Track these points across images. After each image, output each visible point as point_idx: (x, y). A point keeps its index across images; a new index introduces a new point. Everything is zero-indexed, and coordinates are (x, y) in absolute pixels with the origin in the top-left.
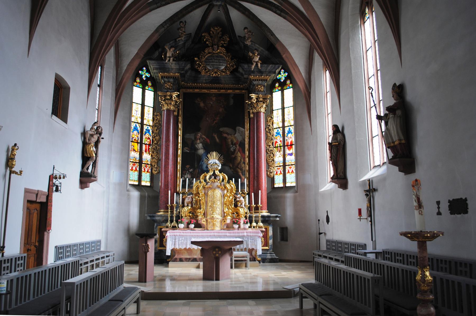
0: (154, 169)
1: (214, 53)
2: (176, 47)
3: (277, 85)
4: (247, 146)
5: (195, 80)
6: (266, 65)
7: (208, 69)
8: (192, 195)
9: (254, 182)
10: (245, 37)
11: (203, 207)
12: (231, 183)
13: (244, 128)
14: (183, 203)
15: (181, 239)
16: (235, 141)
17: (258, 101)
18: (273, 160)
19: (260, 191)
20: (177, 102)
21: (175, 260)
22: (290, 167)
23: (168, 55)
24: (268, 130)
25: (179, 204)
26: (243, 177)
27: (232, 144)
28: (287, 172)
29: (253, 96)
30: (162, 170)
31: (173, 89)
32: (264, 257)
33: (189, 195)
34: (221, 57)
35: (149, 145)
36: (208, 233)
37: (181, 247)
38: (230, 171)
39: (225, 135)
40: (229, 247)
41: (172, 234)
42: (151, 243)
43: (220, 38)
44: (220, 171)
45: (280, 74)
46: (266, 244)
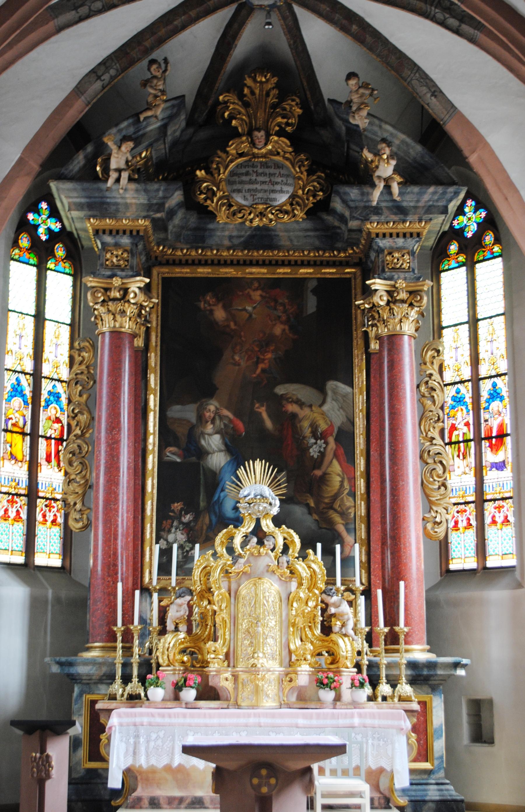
0: (74, 515)
1: (255, 156)
2: (137, 140)
3: (454, 248)
4: (360, 442)
5: (199, 237)
6: (416, 189)
7: (237, 204)
8: (188, 598)
9: (383, 553)
10: (349, 103)
12: (311, 556)
13: (351, 384)
14: (162, 620)
15: (154, 736)
16: (323, 426)
17: (392, 301)
18: (444, 485)
19: (402, 584)
20: (142, 307)
22: (499, 508)
23: (113, 164)
24: (426, 389)
25: (151, 624)
26: (349, 539)
27: (314, 434)
28: (488, 520)
29: (378, 284)
30: (97, 519)
31: (132, 268)
32: (418, 795)
33: (180, 596)
34: (278, 166)
35: (60, 440)
36: (238, 716)
37: (153, 762)
38: (310, 522)
39: (292, 408)
40: (300, 765)
41: (125, 720)
42: (58, 751)
43: (274, 106)
44: (277, 521)
46: (423, 753)
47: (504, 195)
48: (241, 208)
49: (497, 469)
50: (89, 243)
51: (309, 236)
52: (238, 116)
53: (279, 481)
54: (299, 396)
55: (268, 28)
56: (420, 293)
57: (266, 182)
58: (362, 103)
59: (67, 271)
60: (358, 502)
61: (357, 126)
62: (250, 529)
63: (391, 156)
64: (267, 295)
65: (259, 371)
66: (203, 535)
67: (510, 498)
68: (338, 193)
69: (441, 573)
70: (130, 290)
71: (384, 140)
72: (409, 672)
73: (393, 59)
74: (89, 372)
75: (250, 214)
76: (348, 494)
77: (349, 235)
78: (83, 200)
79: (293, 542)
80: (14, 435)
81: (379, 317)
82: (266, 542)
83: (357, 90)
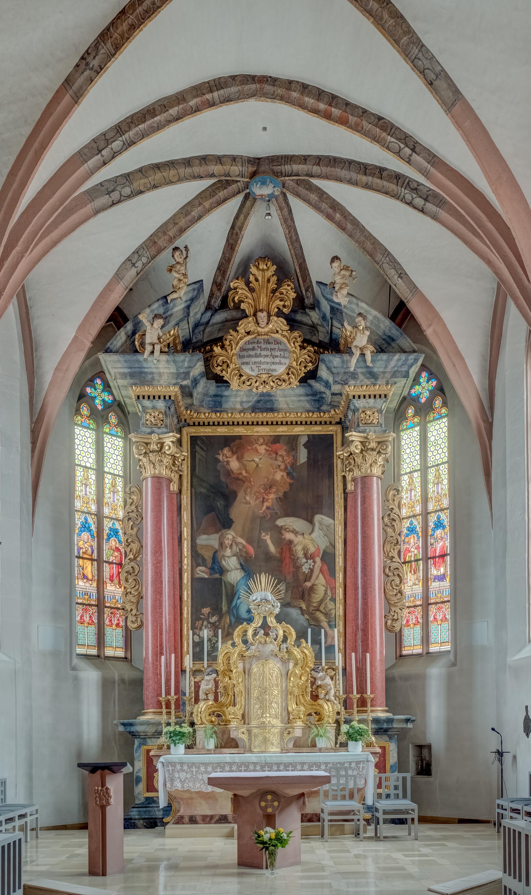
0: (130, 618)
2: (166, 318)
3: (411, 412)
5: (217, 403)
7: (246, 374)
8: (214, 675)
10: (333, 284)
11: (241, 700)
12: (304, 644)
17: (365, 449)
18: (400, 592)
21: (180, 821)
28: (431, 618)
31: (166, 426)
34: (278, 342)
35: (120, 565)
39: (289, 536)
43: (274, 291)
44: (279, 619)
45: (420, 384)
47: (452, 362)
49: (439, 580)
50: (134, 409)
54: (295, 527)
58: (343, 284)
60: (338, 605)
62: (259, 625)
65: (264, 508)
67: (448, 601)
68: (323, 361)
70: (165, 444)
71: (360, 314)
74: (138, 511)
75: (256, 382)
77: (332, 398)
78: (126, 370)
79: (290, 633)
80: (86, 561)
82: (271, 634)
83: (339, 272)
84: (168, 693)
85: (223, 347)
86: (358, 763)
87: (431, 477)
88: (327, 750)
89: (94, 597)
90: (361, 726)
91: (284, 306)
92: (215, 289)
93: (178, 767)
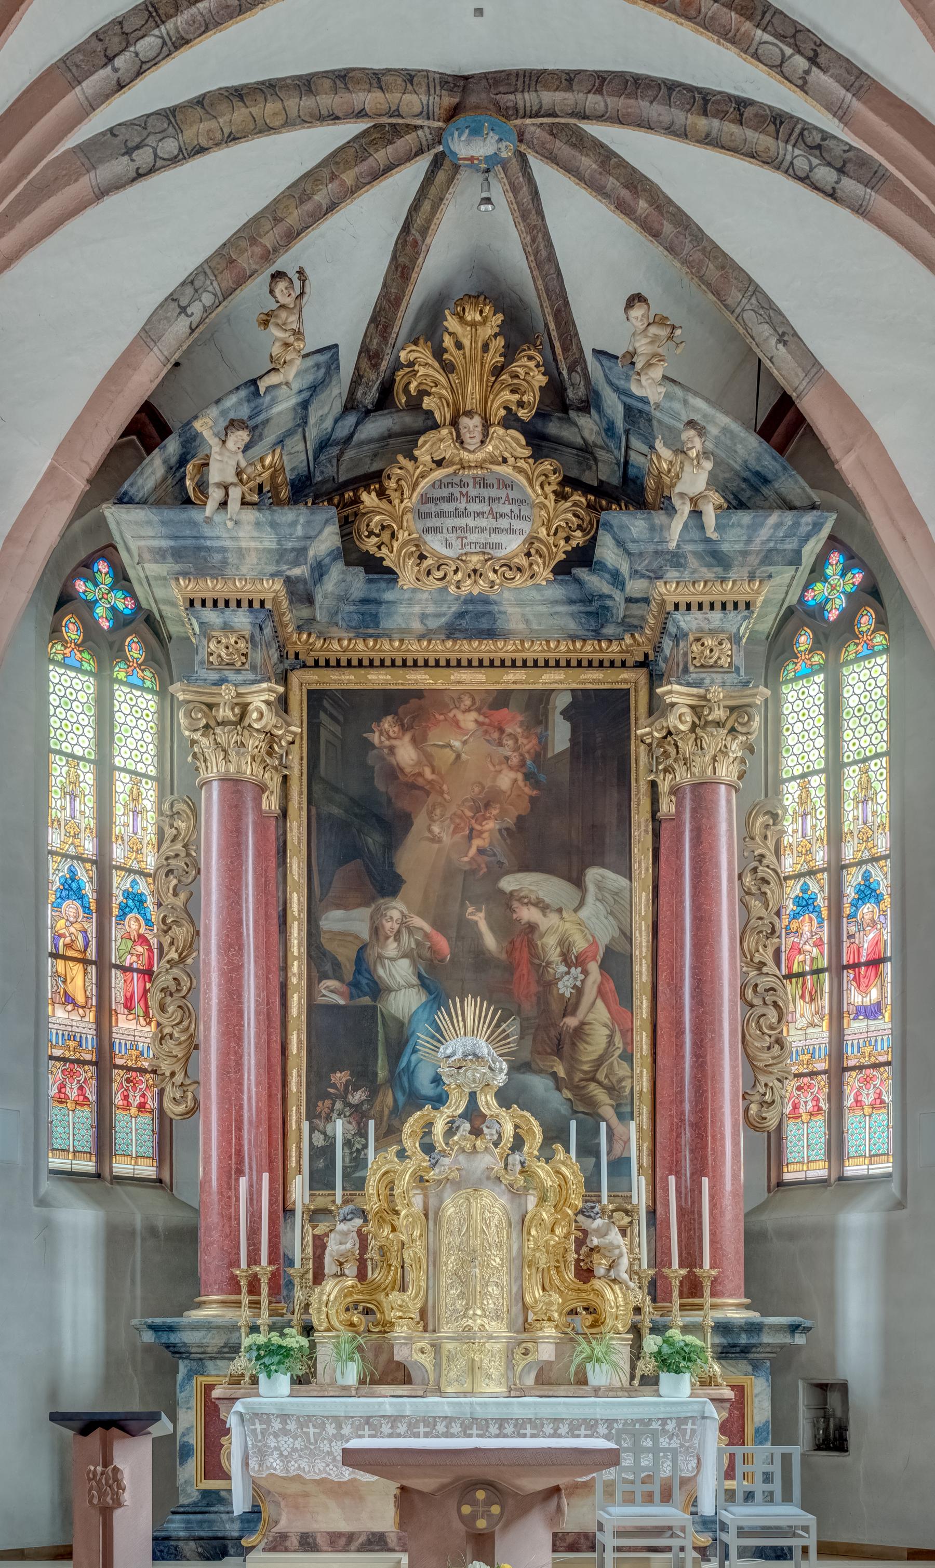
0: (170, 1092)
2: (255, 428)
3: (804, 640)
5: (368, 617)
7: (434, 554)
8: (358, 1222)
10: (630, 357)
11: (417, 1278)
12: (561, 1156)
13: (628, 874)
16: (580, 944)
18: (779, 1042)
21: (278, 1544)
23: (214, 475)
27: (565, 958)
28: (849, 1101)
30: (208, 1096)
31: (253, 668)
34: (508, 485)
35: (148, 973)
39: (528, 914)
43: (497, 371)
44: (505, 1098)
45: (825, 579)
47: (900, 532)
48: (441, 561)
49: (867, 1017)
50: (182, 629)
51: (556, 613)
52: (434, 390)
53: (504, 1031)
54: (541, 895)
55: (486, 211)
56: (748, 709)
57: (483, 513)
58: (654, 355)
59: (148, 684)
60: (637, 1070)
61: (644, 400)
62: (460, 1111)
63: (706, 454)
64: (487, 720)
65: (473, 851)
66: (384, 1124)
67: (888, 1064)
68: (608, 526)
69: (769, 1186)
70: (251, 707)
71: (691, 424)
72: (718, 1340)
73: (711, 271)
74: (188, 855)
75: (456, 572)
76: (620, 1057)
77: (626, 609)
78: (165, 543)
79: (530, 1131)
80: (71, 964)
81: (678, 753)
82: (486, 1130)
84: (254, 1259)
85: (382, 494)
86: (681, 1421)
87: (850, 786)
88: (611, 1391)
89: (90, 1043)
90: (690, 1338)
91: (521, 404)
92: (365, 364)
93: (276, 1425)
